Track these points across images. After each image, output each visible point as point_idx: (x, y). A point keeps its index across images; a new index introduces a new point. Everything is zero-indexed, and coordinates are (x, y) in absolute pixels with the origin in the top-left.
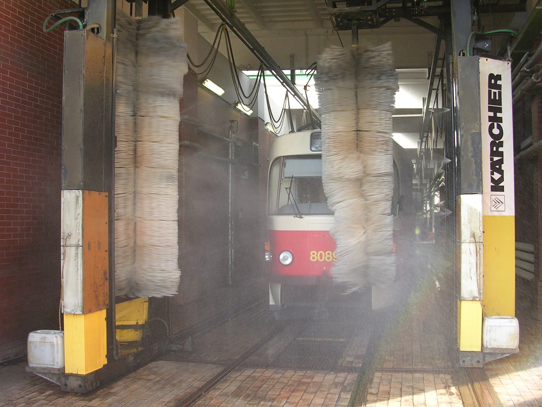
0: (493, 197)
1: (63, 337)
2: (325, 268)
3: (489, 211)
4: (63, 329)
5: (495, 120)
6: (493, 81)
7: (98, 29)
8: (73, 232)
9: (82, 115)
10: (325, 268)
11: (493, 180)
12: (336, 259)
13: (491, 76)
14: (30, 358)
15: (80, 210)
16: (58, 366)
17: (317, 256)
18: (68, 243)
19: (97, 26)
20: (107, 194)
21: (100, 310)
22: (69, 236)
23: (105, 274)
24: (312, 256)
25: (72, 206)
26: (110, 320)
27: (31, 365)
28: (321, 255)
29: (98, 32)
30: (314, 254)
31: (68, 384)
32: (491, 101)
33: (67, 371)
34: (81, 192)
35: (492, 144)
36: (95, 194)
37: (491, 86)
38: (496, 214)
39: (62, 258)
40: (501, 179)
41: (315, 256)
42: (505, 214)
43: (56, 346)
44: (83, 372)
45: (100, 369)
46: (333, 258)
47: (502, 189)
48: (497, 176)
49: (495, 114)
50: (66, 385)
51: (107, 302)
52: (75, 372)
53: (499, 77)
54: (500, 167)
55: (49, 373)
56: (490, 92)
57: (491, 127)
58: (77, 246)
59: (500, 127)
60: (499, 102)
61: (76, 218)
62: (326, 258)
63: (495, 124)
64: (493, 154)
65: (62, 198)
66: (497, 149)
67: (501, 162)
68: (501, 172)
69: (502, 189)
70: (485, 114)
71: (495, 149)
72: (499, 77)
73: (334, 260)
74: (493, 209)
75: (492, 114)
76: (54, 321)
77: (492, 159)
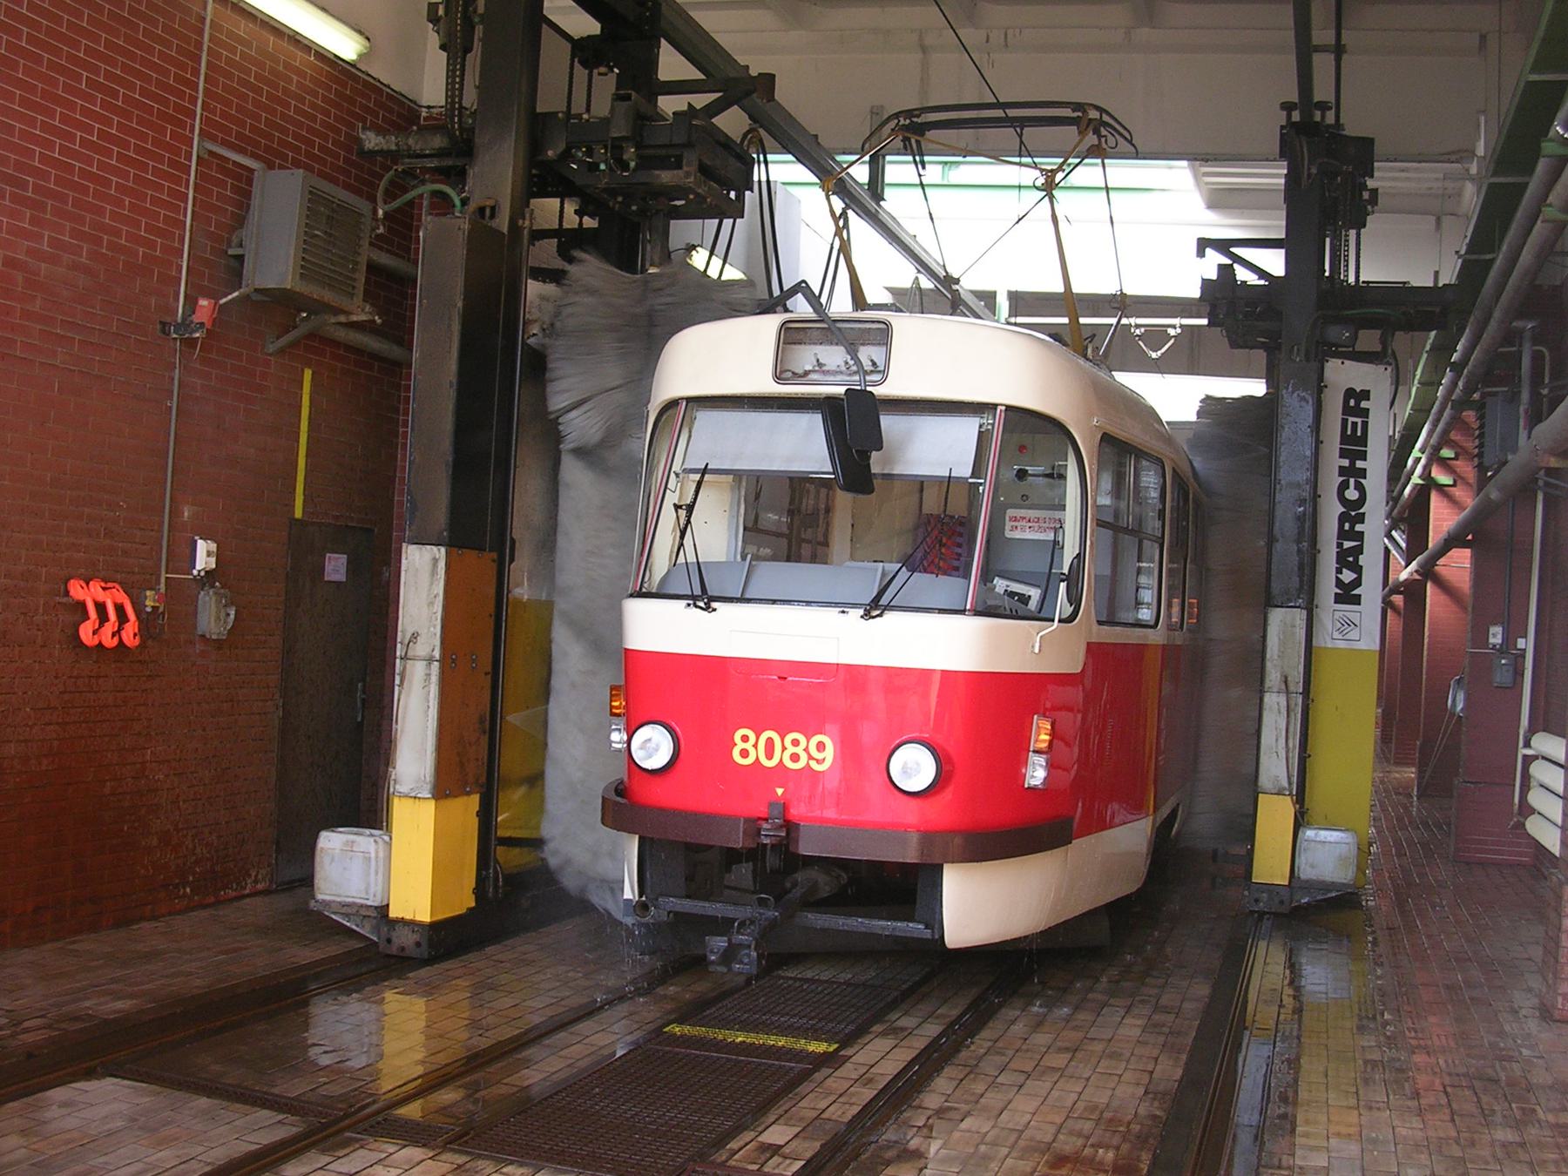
0: (1337, 615)
1: (389, 845)
2: (780, 791)
3: (1328, 639)
4: (389, 830)
5: (1353, 473)
6: (1352, 403)
7: (493, 208)
8: (423, 632)
9: (453, 393)
10: (780, 791)
11: (1339, 583)
12: (818, 761)
13: (1350, 393)
14: (319, 881)
15: (439, 588)
16: (374, 901)
17: (755, 746)
18: (410, 654)
19: (490, 203)
20: (495, 555)
21: (468, 794)
22: (415, 636)
23: (482, 720)
24: (740, 745)
25: (422, 579)
26: (486, 816)
27: (320, 897)
28: (770, 744)
29: (493, 216)
30: (745, 739)
31: (394, 939)
32: (1344, 439)
33: (393, 914)
34: (443, 550)
35: (1342, 518)
36: (471, 555)
37: (1347, 411)
38: (1342, 645)
39: (397, 681)
40: (1357, 583)
41: (749, 746)
42: (1362, 645)
43: (373, 863)
44: (425, 917)
45: (460, 916)
46: (810, 757)
47: (1356, 600)
48: (1348, 576)
49: (1352, 463)
50: (389, 941)
51: (483, 779)
52: (408, 917)
53: (1365, 395)
54: (1356, 560)
55: (357, 914)
56: (1344, 422)
57: (1343, 487)
58: (430, 660)
59: (1360, 488)
60: (1363, 440)
61: (431, 604)
62: (787, 754)
63: (1352, 481)
64: (1343, 535)
65: (404, 561)
66: (1352, 527)
67: (1359, 550)
68: (1357, 569)
69: (1356, 600)
70: (1333, 460)
71: (1347, 526)
72: (1365, 395)
73: (813, 764)
74: (1336, 635)
75: (1346, 463)
76: (366, 808)
77: (1340, 545)
